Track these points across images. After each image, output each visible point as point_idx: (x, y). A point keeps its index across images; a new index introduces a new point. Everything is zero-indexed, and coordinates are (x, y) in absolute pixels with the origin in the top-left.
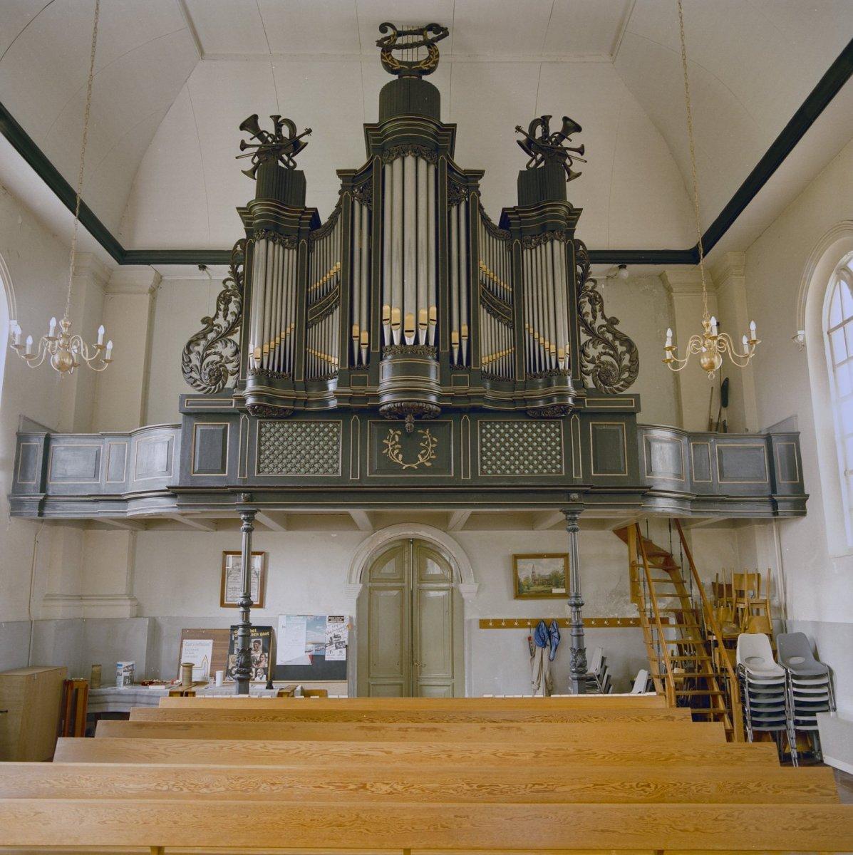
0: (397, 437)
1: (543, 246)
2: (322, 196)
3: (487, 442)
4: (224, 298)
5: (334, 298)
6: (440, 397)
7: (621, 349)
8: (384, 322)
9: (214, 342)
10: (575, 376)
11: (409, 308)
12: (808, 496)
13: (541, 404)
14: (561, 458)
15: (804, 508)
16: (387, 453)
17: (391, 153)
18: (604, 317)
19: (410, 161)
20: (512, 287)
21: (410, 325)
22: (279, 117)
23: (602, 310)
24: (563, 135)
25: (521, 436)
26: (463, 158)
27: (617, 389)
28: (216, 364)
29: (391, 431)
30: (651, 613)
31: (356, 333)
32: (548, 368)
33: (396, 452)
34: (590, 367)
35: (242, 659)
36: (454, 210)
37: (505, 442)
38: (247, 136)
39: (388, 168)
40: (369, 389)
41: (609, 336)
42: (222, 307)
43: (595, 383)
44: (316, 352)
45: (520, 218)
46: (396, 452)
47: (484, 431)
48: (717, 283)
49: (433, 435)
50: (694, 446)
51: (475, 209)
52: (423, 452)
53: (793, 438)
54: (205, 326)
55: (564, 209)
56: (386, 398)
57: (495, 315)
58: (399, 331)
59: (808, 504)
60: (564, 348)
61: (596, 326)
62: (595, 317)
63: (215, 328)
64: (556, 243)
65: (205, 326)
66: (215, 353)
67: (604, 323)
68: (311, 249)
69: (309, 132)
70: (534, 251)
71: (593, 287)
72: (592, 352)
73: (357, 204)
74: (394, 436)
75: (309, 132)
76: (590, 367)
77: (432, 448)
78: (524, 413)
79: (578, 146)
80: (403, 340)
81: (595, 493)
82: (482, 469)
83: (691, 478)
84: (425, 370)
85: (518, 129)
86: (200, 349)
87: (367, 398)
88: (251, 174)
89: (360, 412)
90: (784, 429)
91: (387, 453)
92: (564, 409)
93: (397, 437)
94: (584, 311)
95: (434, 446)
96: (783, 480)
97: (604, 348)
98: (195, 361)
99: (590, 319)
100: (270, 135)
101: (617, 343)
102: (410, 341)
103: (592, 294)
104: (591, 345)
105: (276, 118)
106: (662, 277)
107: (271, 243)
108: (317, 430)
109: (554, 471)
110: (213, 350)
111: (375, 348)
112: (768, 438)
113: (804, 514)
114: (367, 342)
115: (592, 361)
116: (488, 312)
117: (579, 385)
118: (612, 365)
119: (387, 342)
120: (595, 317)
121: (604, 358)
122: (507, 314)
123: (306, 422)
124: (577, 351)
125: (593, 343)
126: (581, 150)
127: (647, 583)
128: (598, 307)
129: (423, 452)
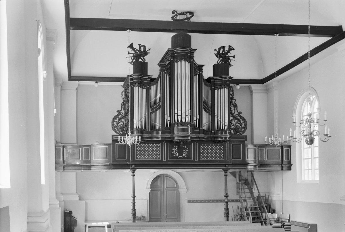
0: (176, 148)
1: (221, 90)
2: (154, 71)
3: (202, 149)
4: (123, 104)
5: (159, 106)
6: (191, 138)
7: (242, 122)
8: (175, 114)
9: (121, 118)
10: (229, 131)
11: (183, 110)
12: (292, 164)
13: (220, 139)
14: (223, 155)
15: (291, 168)
16: (174, 153)
17: (177, 60)
18: (237, 111)
19: (183, 62)
20: (211, 102)
21: (183, 116)
22: (140, 44)
23: (237, 109)
24: (229, 51)
25: (212, 148)
26: (198, 62)
27: (240, 134)
28: (122, 125)
29: (175, 146)
30: (244, 198)
31: (166, 117)
32: (222, 128)
33: (176, 152)
34: (233, 127)
35: (134, 212)
36: (195, 77)
37: (205, 150)
38: (130, 50)
39: (176, 64)
40: (171, 135)
41: (239, 118)
42: (123, 107)
43: (234, 132)
44: (159, 125)
45: (214, 80)
46: (176, 152)
47: (201, 146)
48: (267, 90)
49: (187, 147)
50: (260, 149)
51: (201, 76)
52: (184, 152)
53: (289, 147)
54: (118, 113)
55: (228, 78)
56: (176, 138)
57: (206, 111)
58: (180, 118)
59: (292, 167)
60: (226, 123)
61: (235, 114)
62: (235, 111)
63: (121, 114)
64: (225, 89)
65: (118, 113)
66: (122, 122)
67: (237, 113)
68: (150, 89)
69: (150, 49)
70: (218, 91)
71: (235, 102)
72: (234, 122)
73: (165, 74)
74: (176, 148)
75: (150, 49)
76: (233, 127)
77: (187, 152)
78: (214, 141)
79: (233, 56)
80: (181, 121)
81: (234, 165)
82: (201, 158)
83: (259, 159)
84: (187, 130)
85: (215, 50)
86: (117, 120)
87: (170, 138)
88: (131, 63)
89: (170, 141)
90: (287, 144)
91: (174, 153)
92: (226, 141)
93: (176, 148)
94: (232, 110)
95: (187, 151)
96: (285, 159)
97: (237, 121)
98: (115, 125)
99: (233, 112)
100: (137, 50)
101: (241, 120)
102: (183, 121)
103: (234, 104)
104: (233, 120)
105: (139, 45)
106: (249, 88)
107: (139, 88)
108: (153, 146)
109: (221, 158)
110: (121, 121)
111: (172, 122)
112: (282, 147)
113: (291, 170)
114: (169, 120)
115: (233, 125)
116: (204, 110)
117: (230, 133)
118: (239, 127)
119: (176, 121)
120: (235, 111)
121: (237, 124)
122: (210, 111)
123: (152, 144)
124: (230, 122)
125: (234, 120)
126: (234, 57)
127: (243, 189)
128: (236, 108)
129: (184, 152)
